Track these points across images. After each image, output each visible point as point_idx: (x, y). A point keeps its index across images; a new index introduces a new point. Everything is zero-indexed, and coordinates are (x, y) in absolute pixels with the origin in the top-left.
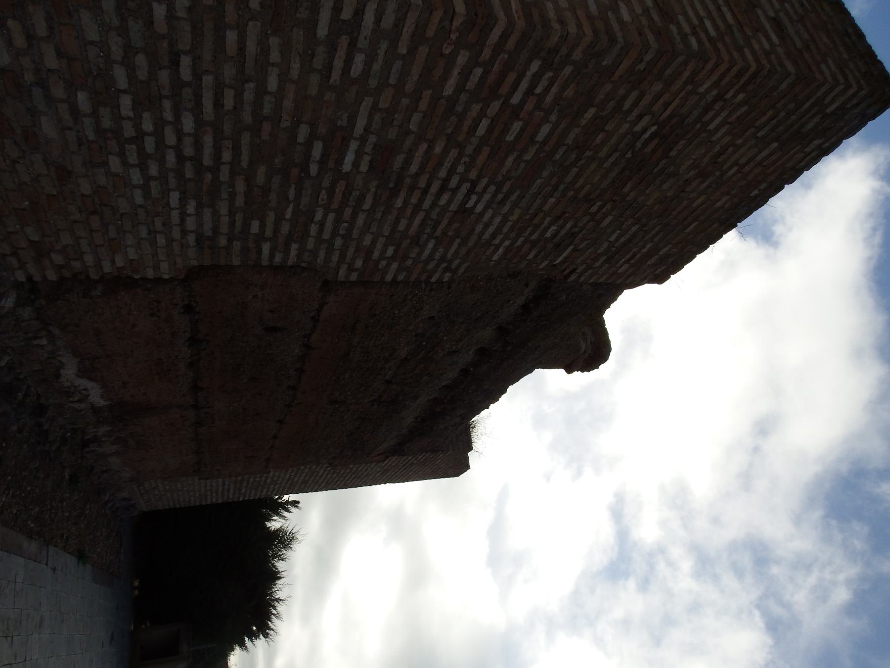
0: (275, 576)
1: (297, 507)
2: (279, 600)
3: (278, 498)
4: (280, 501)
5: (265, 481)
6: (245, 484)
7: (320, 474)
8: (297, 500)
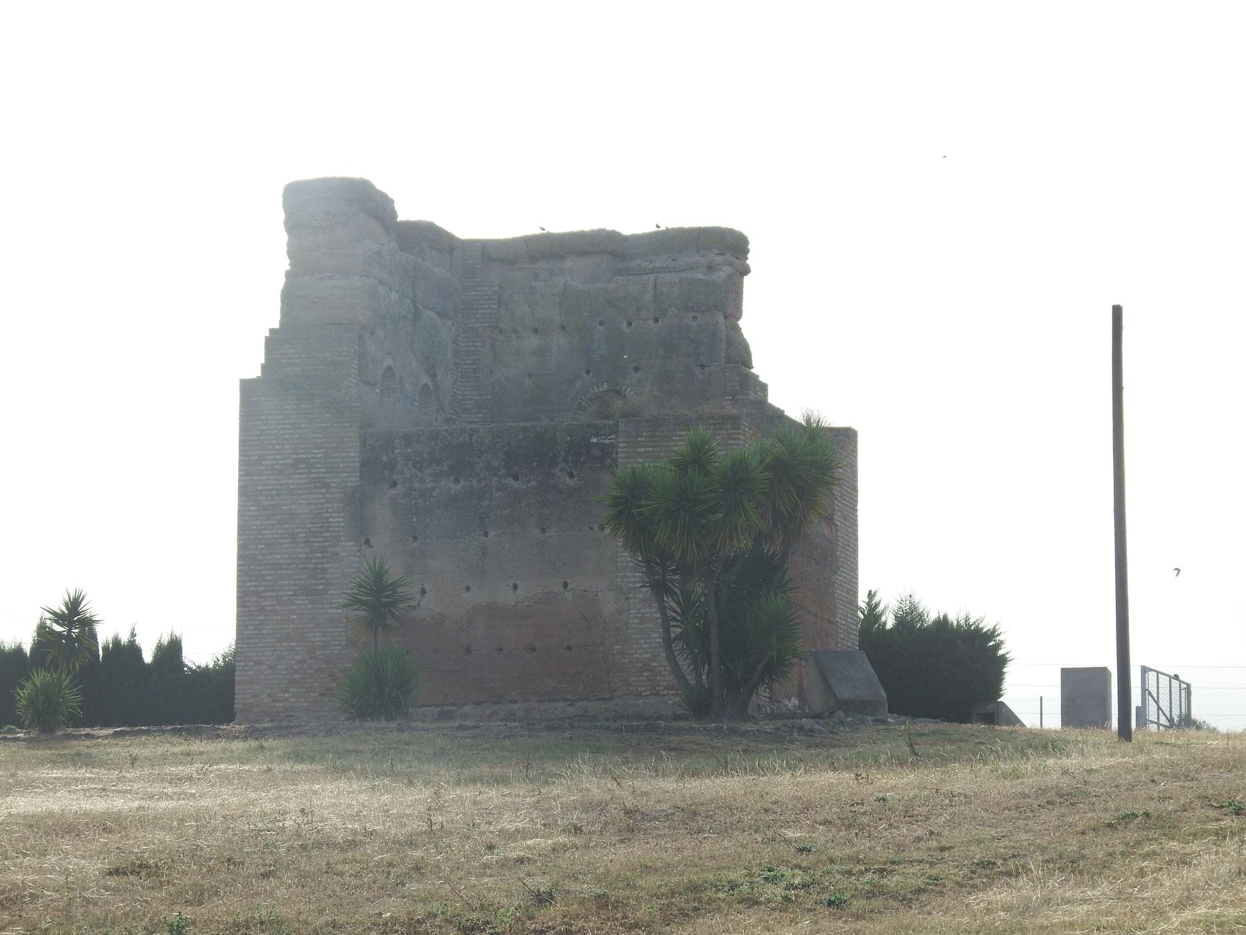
0: (943, 623)
1: (875, 594)
2: (967, 619)
3: (863, 613)
4: (866, 612)
5: (844, 625)
6: (844, 642)
7: (842, 579)
8: (868, 592)
